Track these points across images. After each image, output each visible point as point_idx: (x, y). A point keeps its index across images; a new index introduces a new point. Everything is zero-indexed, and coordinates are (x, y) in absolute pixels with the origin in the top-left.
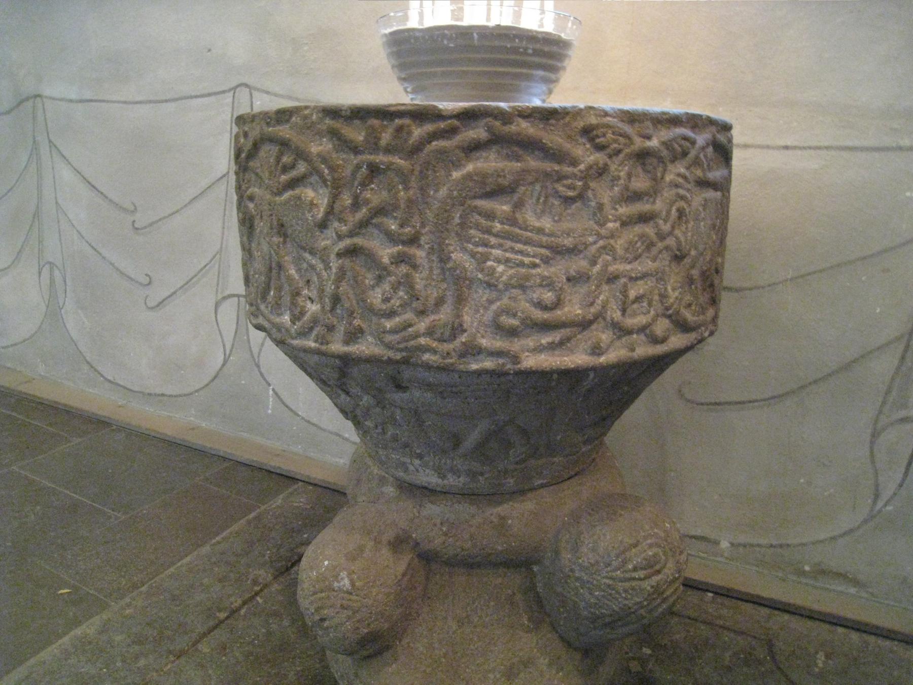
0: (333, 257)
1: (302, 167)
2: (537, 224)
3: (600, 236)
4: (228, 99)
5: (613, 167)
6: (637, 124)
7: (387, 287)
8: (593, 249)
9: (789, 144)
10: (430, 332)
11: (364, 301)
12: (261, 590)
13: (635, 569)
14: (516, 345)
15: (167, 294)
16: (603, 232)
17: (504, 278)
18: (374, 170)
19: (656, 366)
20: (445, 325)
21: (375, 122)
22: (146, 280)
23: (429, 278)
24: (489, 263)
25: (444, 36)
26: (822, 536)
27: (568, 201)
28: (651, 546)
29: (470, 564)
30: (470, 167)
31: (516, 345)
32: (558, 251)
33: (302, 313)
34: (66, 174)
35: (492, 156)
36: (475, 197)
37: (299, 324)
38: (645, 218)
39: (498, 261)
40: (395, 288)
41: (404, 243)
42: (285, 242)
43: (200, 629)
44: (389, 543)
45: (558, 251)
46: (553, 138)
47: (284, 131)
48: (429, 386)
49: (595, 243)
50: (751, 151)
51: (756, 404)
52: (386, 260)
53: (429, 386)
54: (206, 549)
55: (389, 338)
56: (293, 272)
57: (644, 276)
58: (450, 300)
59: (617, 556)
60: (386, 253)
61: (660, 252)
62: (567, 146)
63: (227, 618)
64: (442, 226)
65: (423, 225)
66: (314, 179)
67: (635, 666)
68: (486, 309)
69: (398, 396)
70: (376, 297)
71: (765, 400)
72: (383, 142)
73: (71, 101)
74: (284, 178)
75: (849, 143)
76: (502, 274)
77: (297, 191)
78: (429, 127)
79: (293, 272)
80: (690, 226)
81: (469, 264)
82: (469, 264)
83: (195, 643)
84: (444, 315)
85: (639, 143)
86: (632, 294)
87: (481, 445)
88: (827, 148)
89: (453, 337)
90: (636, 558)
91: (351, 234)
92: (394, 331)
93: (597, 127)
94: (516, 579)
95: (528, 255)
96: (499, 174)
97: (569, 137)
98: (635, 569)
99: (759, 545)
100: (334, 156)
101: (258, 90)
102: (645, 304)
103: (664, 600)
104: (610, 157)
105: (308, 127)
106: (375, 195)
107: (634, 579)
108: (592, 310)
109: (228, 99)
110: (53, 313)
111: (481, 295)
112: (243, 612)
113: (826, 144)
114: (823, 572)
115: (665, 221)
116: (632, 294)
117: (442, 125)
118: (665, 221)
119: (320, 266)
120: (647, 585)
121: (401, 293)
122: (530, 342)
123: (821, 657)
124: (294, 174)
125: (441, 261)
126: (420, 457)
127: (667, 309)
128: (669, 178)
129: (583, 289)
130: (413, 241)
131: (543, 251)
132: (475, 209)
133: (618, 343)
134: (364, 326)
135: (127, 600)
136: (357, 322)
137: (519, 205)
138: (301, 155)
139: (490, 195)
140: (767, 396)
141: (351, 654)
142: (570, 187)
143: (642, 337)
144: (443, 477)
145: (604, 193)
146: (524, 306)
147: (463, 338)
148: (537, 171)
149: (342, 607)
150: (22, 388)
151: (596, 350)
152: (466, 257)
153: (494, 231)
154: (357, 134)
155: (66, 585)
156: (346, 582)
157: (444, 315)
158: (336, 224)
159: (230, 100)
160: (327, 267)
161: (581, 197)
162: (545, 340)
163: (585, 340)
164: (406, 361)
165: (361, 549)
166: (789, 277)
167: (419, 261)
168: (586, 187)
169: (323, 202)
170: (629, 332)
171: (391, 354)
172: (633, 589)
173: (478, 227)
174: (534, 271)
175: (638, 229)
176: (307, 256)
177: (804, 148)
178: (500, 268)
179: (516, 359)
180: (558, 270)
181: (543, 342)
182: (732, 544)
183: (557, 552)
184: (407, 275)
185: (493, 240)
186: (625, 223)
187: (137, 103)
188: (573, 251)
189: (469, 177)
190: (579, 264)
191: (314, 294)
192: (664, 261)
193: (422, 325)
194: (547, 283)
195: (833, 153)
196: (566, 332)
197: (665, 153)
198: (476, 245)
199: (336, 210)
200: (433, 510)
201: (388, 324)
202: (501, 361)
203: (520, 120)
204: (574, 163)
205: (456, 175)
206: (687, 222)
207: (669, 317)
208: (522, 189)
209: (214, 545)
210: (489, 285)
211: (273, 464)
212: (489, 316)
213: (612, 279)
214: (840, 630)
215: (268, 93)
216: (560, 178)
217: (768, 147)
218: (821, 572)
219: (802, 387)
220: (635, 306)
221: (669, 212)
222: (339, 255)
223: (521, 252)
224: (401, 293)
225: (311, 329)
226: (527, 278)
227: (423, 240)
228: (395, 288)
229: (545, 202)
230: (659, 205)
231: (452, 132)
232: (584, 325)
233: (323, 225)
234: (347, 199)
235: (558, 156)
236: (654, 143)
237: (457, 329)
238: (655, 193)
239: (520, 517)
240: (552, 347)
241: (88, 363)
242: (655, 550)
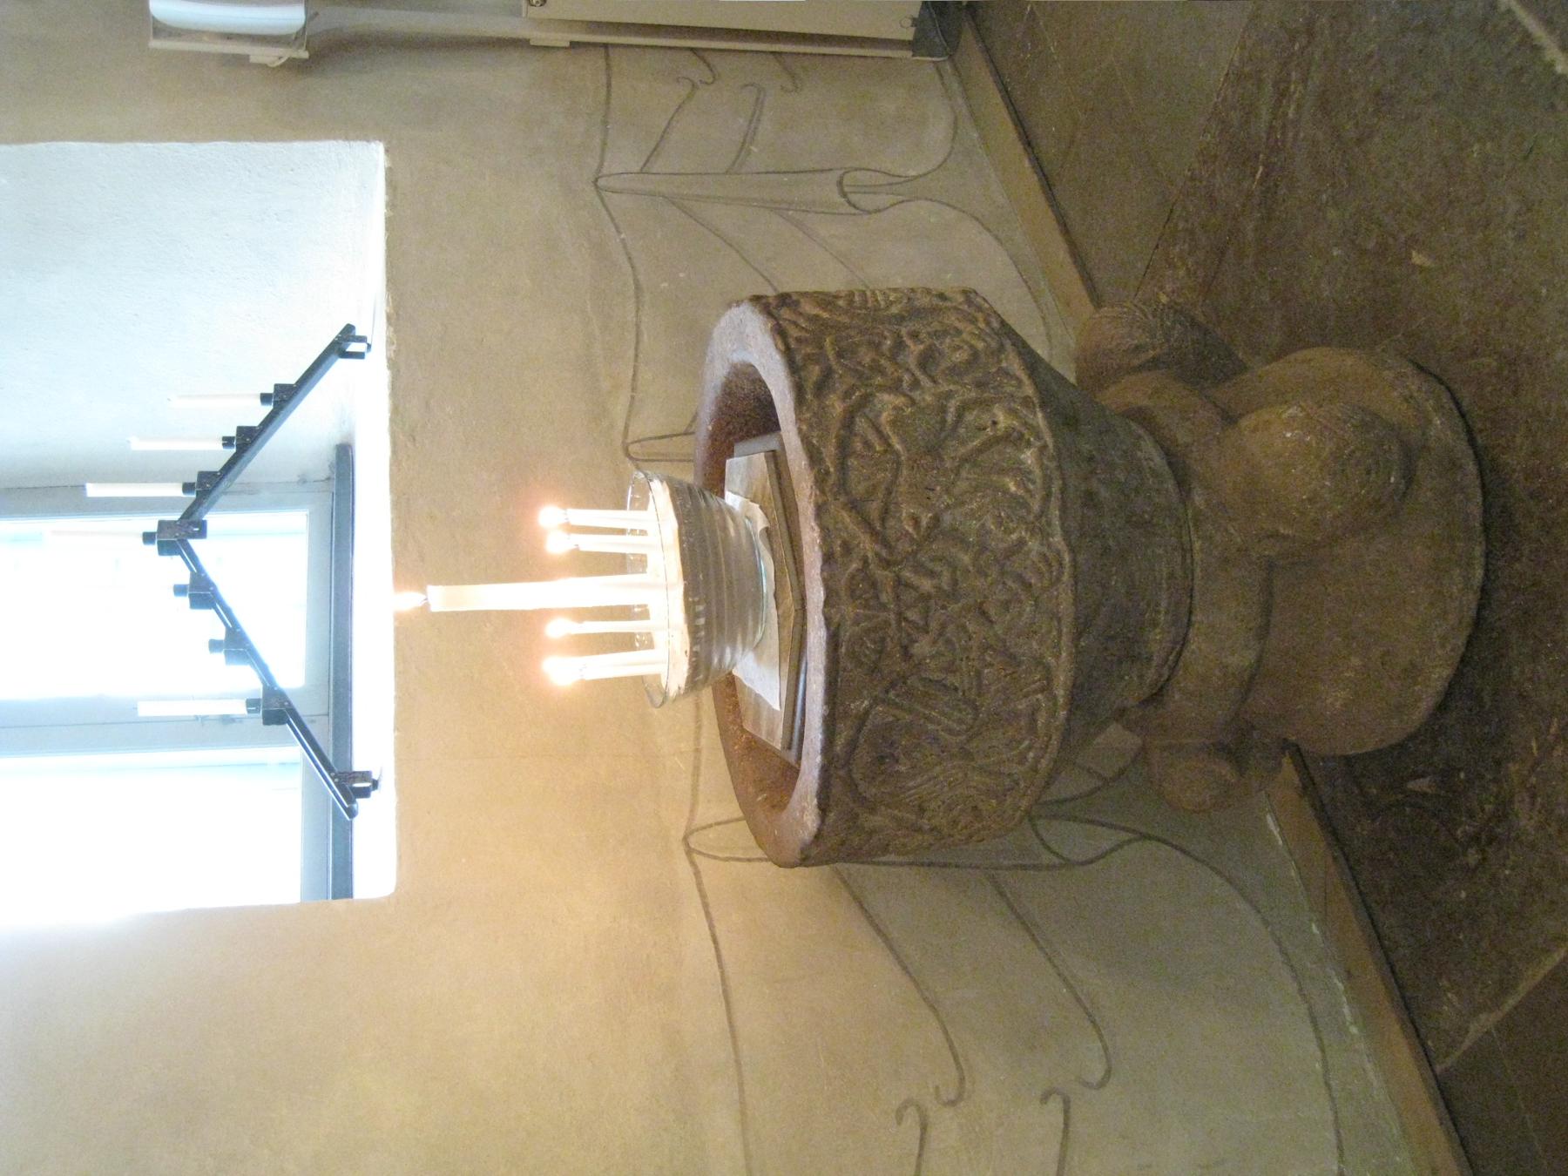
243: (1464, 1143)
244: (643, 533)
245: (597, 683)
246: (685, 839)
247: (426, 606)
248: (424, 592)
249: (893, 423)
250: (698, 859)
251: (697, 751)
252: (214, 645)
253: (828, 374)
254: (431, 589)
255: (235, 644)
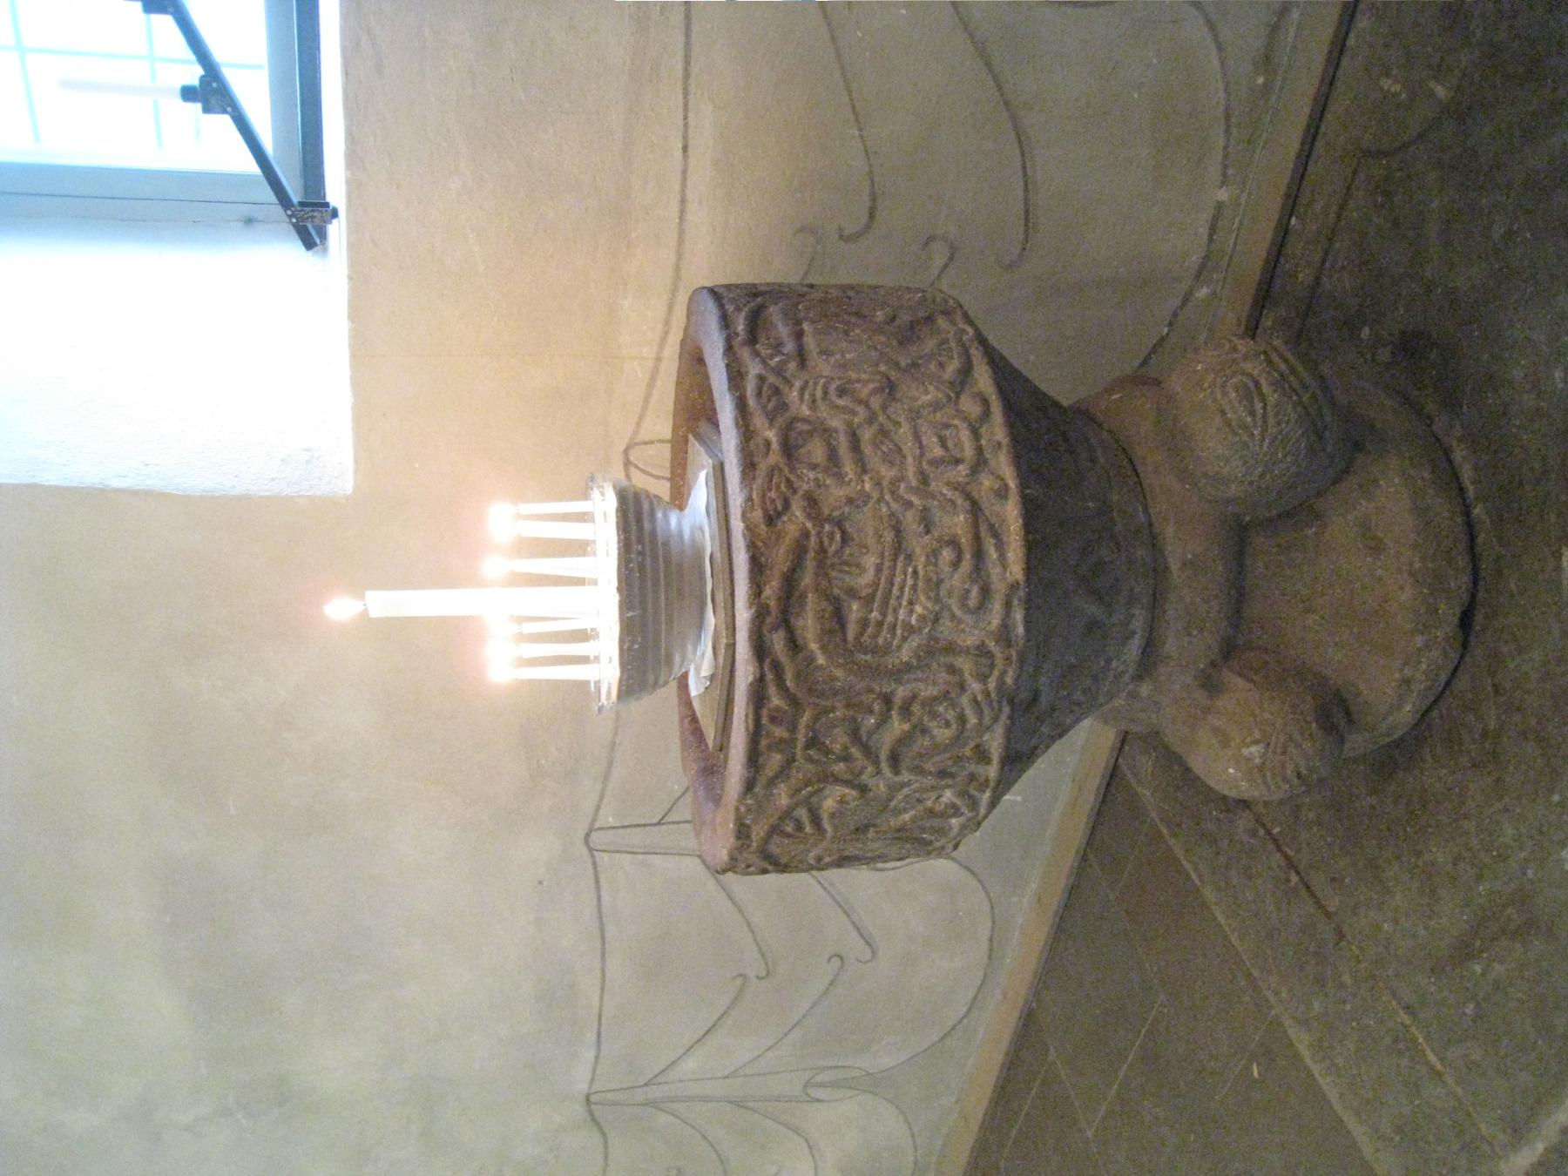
0: (897, 779)
1: (802, 813)
2: (871, 572)
3: (880, 500)
4: (604, 858)
5: (805, 487)
6: (756, 459)
7: (933, 724)
8: (894, 506)
9: (680, 146)
10: (983, 678)
11: (946, 746)
12: (1264, 825)
13: (1252, 413)
14: (999, 588)
15: (855, 933)
16: (875, 495)
17: (929, 605)
18: (812, 742)
19: (1004, 373)
20: (976, 663)
21: (764, 742)
22: (836, 962)
23: (925, 681)
24: (913, 621)
25: (629, 649)
26: (1216, 63)
27: (845, 539)
28: (1225, 394)
29: (1238, 597)
30: (814, 646)
31: (999, 588)
32: (898, 548)
33: (954, 806)
34: (691, 1065)
35: (801, 623)
36: (845, 641)
37: (964, 810)
38: (855, 445)
39: (912, 611)
40: (934, 715)
41: (889, 710)
42: (875, 825)
43: (1310, 908)
44: (1211, 697)
45: (898, 548)
46: (780, 558)
47: (758, 832)
48: (1038, 668)
49: (887, 504)
50: (690, 196)
51: (1028, 164)
52: (906, 727)
53: (1038, 668)
54: (1209, 893)
55: (987, 721)
56: (907, 817)
57: (917, 437)
58: (949, 660)
59: (1235, 434)
60: (898, 726)
61: (888, 417)
62: (788, 541)
63: (1298, 873)
64: (875, 672)
65: (871, 691)
66: (814, 800)
67: (1384, 355)
68: (960, 621)
69: (1044, 701)
70: (942, 734)
71: (1023, 154)
72: (785, 735)
73: (597, 1057)
74: (808, 829)
75: (680, 66)
76: (925, 608)
77: (825, 817)
78: (772, 690)
79: (907, 817)
80: (854, 376)
81: (915, 641)
82: (915, 641)
83: (1328, 915)
84: (965, 664)
85: (775, 457)
86: (938, 452)
87: (1098, 596)
88: (686, 94)
89: (990, 655)
90: (1238, 413)
91: (877, 762)
92: (980, 713)
93: (765, 511)
94: (1258, 541)
95: (904, 581)
96: (820, 617)
97: (778, 539)
98: (1252, 413)
99: (1225, 148)
100: (793, 781)
101: (594, 820)
102: (948, 433)
103: (1293, 371)
104: (795, 492)
105: (760, 809)
106: (838, 740)
107: (1264, 415)
108: (959, 501)
109: (604, 858)
110: (873, 1084)
111: (945, 628)
112: (1291, 853)
113: (681, 97)
114: (1267, 58)
115: (854, 413)
116: (938, 452)
117: (770, 676)
118: (854, 413)
119: (906, 791)
120: (1272, 399)
121: (941, 709)
122: (995, 571)
123: (1386, 84)
124: (806, 820)
125: (909, 671)
126: (1108, 661)
127: (949, 398)
128: (805, 411)
129: (937, 514)
130: (887, 700)
131: (900, 564)
132: (858, 638)
133: (993, 463)
134: (972, 744)
135: (1269, 994)
136: (967, 752)
137: (852, 593)
138: (787, 814)
139: (842, 624)
140: (1018, 152)
141: (1342, 740)
142: (832, 539)
143: (983, 430)
144: (1134, 632)
145: (834, 495)
146: (956, 580)
147: (991, 644)
148: (817, 575)
149: (1284, 753)
150: (975, 1124)
151: (1002, 493)
152: (906, 646)
153: (880, 618)
154: (775, 760)
155: (1248, 1068)
156: (1254, 749)
157: (965, 664)
158: (864, 777)
159: (606, 856)
160: (908, 784)
161: (839, 523)
162: (993, 554)
163: (990, 506)
164: (1011, 702)
165: (1216, 730)
166: (857, 133)
167: (908, 693)
168: (829, 519)
169: (840, 790)
170: (980, 450)
171: (1004, 718)
172: (1277, 415)
173: (875, 636)
174: (921, 573)
175: (867, 450)
176: (892, 804)
177: (686, 125)
178: (918, 609)
179: (1014, 587)
180: (919, 545)
181: (995, 556)
182: (1223, 183)
183: (1228, 501)
184: (923, 705)
185: (890, 618)
186: (863, 469)
187: (603, 975)
188: (898, 530)
189: (823, 648)
190: (910, 519)
191: (933, 795)
192: (899, 411)
193: (975, 686)
194: (934, 554)
195: (692, 89)
196: (983, 530)
197: (780, 420)
198: (894, 636)
199: (848, 777)
200: (1171, 646)
201: (973, 720)
202: (1016, 602)
203: (764, 596)
204: (806, 534)
205: (821, 660)
206: (850, 381)
207: (958, 395)
208: (836, 591)
209: (1202, 881)
210: (936, 620)
211: (1092, 798)
212: (969, 619)
213: (924, 479)
214: (1351, 42)
215: (598, 808)
216: (822, 550)
217: (684, 172)
218: (1266, 61)
219: (1006, 103)
220: (950, 444)
221: (844, 409)
222: (897, 772)
223: (902, 589)
224: (941, 709)
225: (970, 797)
226: (929, 580)
227: (886, 689)
228: (934, 715)
229: (847, 564)
230: (836, 423)
231: (777, 667)
232: (975, 509)
233: (863, 789)
234: (839, 768)
235: (800, 551)
236: (771, 435)
237: (982, 651)
238: (825, 431)
239: (1184, 545)
240: (1000, 546)
241: (942, 1039)
242: (1229, 389)
243: (1099, 813)
244: (594, 582)
245: (522, 682)
246: (626, 452)
247: (366, 612)
248: (361, 597)
249: (832, 816)
250: (632, 469)
251: (658, 359)
252: (188, 94)
253: (790, 761)
254: (370, 594)
255: (211, 92)
